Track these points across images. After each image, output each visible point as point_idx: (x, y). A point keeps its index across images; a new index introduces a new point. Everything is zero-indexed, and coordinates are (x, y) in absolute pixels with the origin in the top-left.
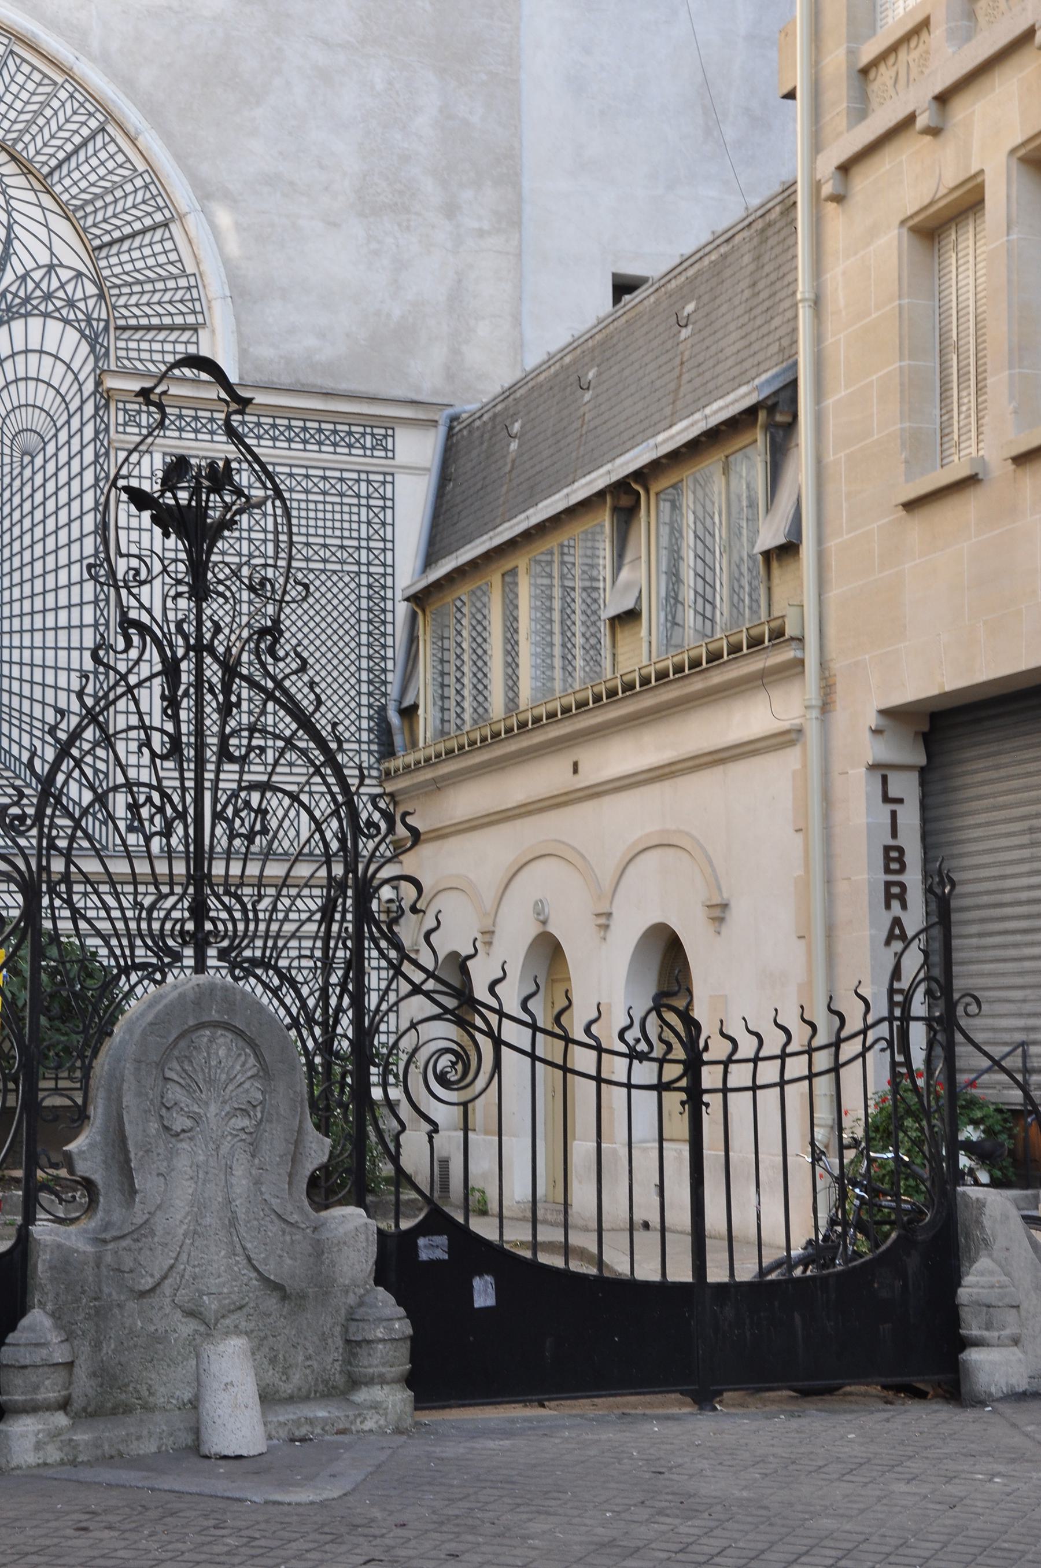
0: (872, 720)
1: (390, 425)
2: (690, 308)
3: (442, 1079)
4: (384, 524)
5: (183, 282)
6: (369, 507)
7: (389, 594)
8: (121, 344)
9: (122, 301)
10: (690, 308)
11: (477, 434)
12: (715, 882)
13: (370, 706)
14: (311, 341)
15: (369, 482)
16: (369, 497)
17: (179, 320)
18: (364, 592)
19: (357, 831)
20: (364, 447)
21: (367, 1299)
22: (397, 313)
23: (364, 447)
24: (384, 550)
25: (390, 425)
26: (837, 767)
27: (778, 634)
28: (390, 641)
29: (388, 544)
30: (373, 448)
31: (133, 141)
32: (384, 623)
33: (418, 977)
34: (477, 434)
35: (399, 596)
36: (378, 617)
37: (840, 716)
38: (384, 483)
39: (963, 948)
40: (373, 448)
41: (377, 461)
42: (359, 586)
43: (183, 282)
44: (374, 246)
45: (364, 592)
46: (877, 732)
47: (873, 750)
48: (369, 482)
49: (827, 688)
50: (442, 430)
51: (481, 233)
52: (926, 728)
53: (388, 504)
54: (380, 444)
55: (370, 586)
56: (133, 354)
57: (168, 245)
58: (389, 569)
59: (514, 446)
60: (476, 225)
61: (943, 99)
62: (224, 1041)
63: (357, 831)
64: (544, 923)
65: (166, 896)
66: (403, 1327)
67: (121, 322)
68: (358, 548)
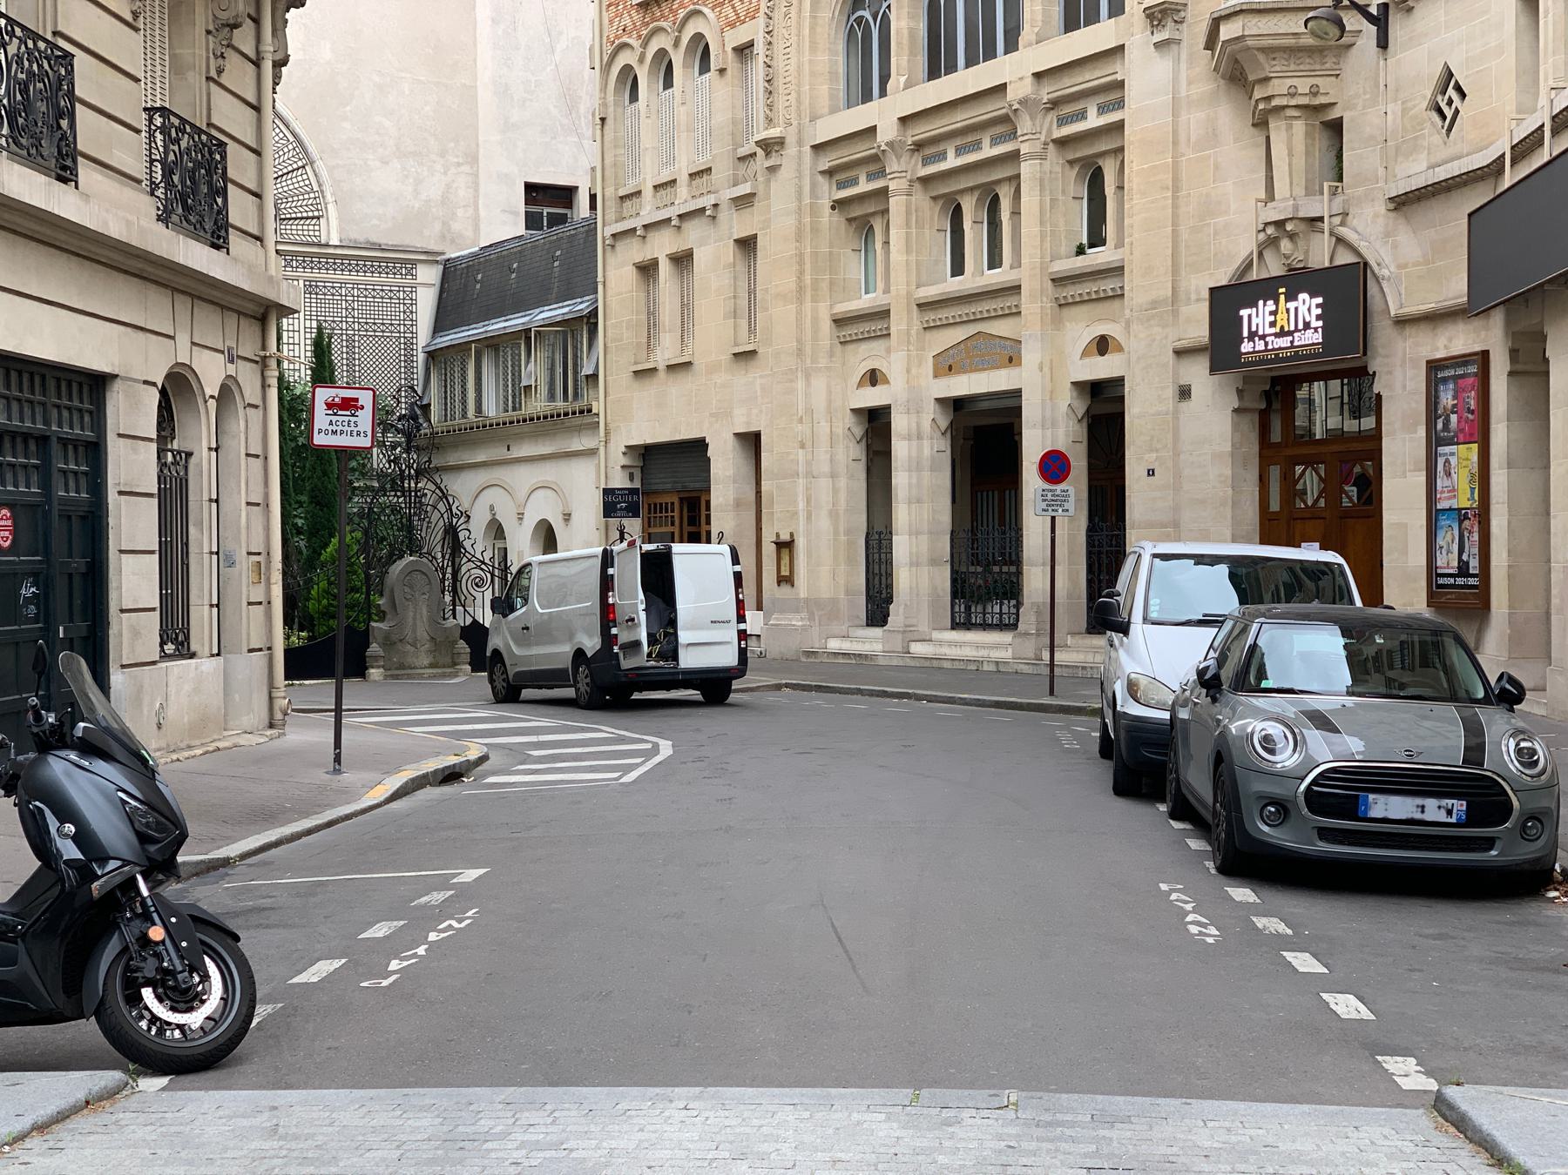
0: (624, 449)
1: (414, 263)
2: (558, 253)
3: (477, 585)
4: (412, 312)
5: (312, 195)
6: (404, 304)
7: (415, 347)
8: (283, 227)
9: (283, 206)
10: (558, 253)
11: (459, 272)
13: (406, 403)
14: (375, 222)
15: (404, 292)
16: (404, 299)
17: (310, 214)
18: (402, 346)
19: (452, 515)
20: (401, 274)
22: (417, 205)
23: (401, 274)
24: (412, 325)
25: (414, 263)
26: (610, 465)
27: (590, 411)
28: (415, 377)
29: (414, 323)
30: (406, 275)
31: (287, 127)
32: (412, 361)
33: (470, 557)
34: (459, 272)
35: (420, 350)
36: (409, 359)
37: (612, 446)
38: (412, 292)
40: (406, 275)
41: (408, 281)
42: (400, 343)
43: (312, 195)
44: (405, 173)
45: (402, 346)
46: (624, 454)
47: (624, 461)
48: (404, 292)
49: (607, 433)
50: (441, 267)
51: (459, 164)
52: (643, 451)
53: (414, 302)
54: (409, 273)
55: (405, 344)
56: (289, 232)
57: (305, 177)
58: (414, 335)
59: (478, 286)
60: (456, 160)
61: (645, 227)
62: (419, 576)
63: (452, 515)
64: (494, 515)
66: (468, 650)
67: (283, 217)
68: (399, 325)
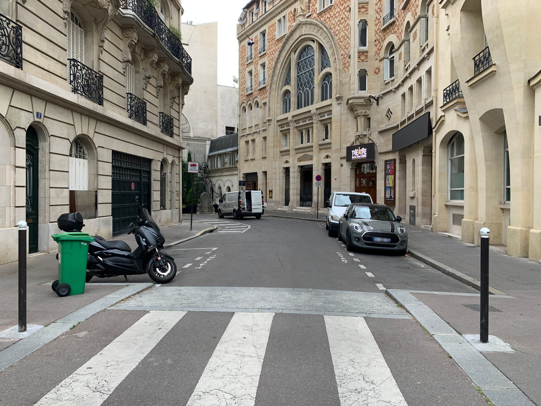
1: (206, 140)
12: (232, 183)
21: (245, 98)
25: (206, 140)
29: (206, 151)
36: (205, 157)
37: (241, 173)
39: (324, 150)
41: (205, 143)
47: (243, 176)
49: (240, 171)
53: (206, 147)
54: (205, 142)
58: (206, 153)
65: (291, 375)
